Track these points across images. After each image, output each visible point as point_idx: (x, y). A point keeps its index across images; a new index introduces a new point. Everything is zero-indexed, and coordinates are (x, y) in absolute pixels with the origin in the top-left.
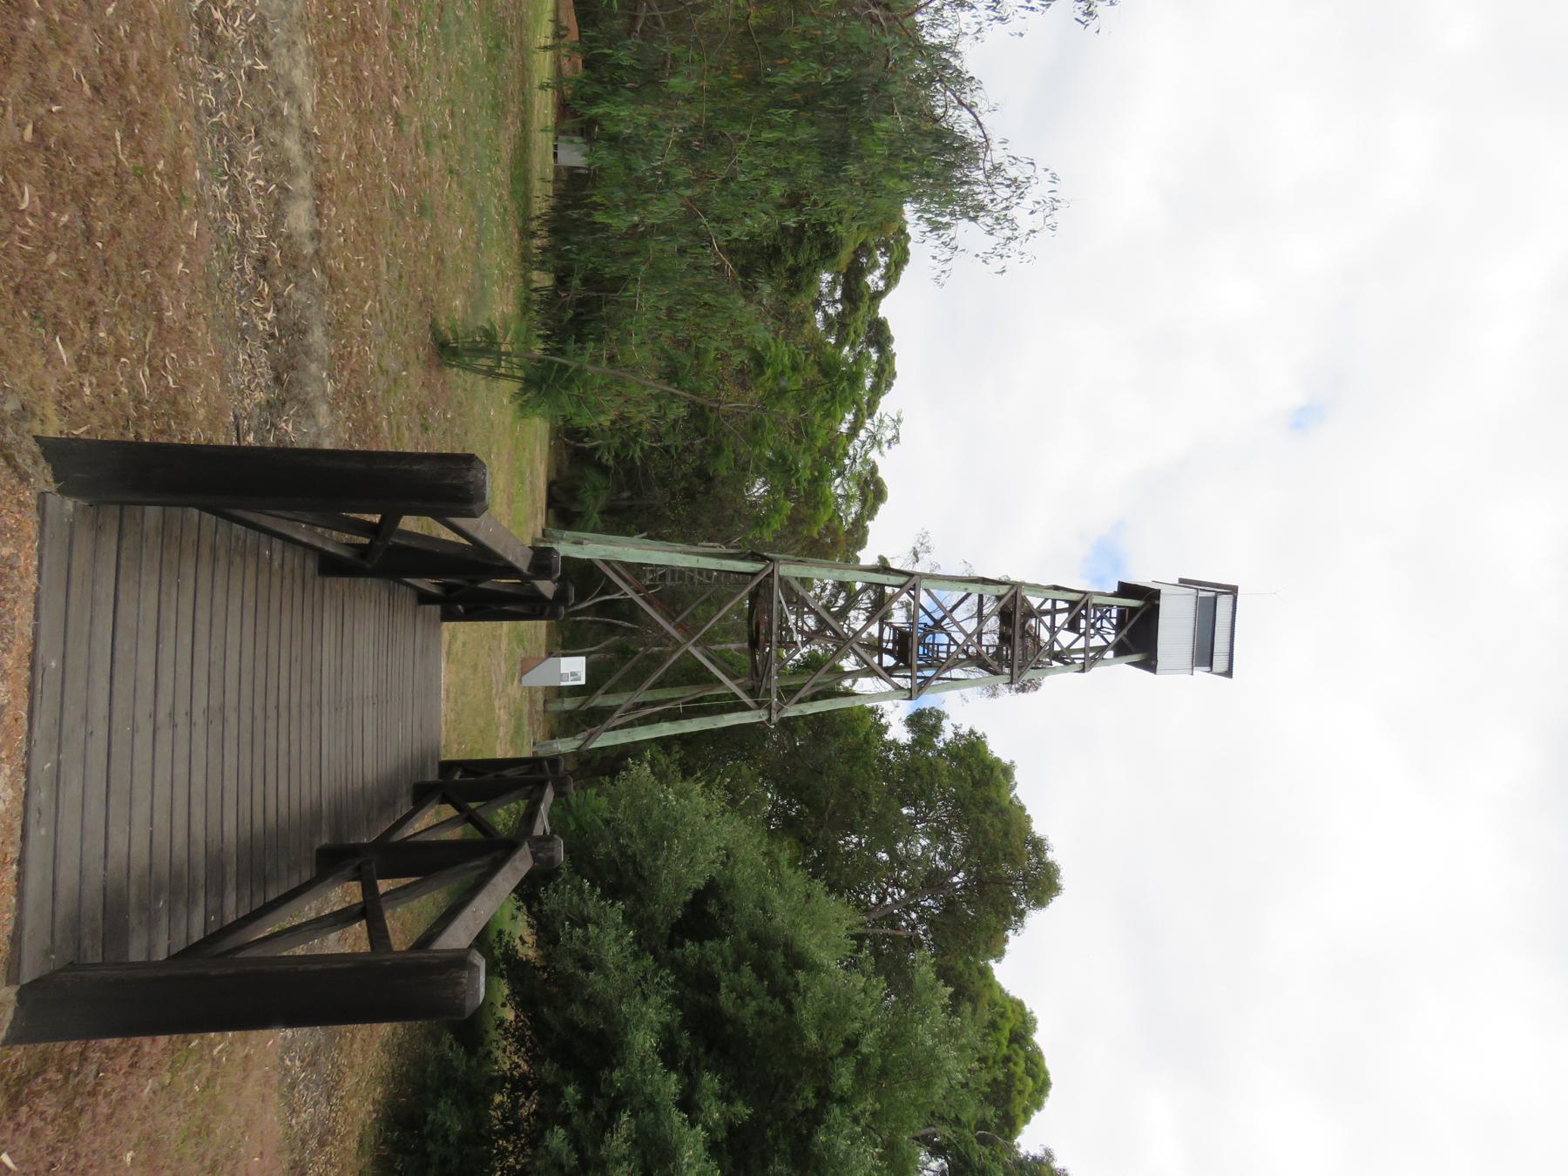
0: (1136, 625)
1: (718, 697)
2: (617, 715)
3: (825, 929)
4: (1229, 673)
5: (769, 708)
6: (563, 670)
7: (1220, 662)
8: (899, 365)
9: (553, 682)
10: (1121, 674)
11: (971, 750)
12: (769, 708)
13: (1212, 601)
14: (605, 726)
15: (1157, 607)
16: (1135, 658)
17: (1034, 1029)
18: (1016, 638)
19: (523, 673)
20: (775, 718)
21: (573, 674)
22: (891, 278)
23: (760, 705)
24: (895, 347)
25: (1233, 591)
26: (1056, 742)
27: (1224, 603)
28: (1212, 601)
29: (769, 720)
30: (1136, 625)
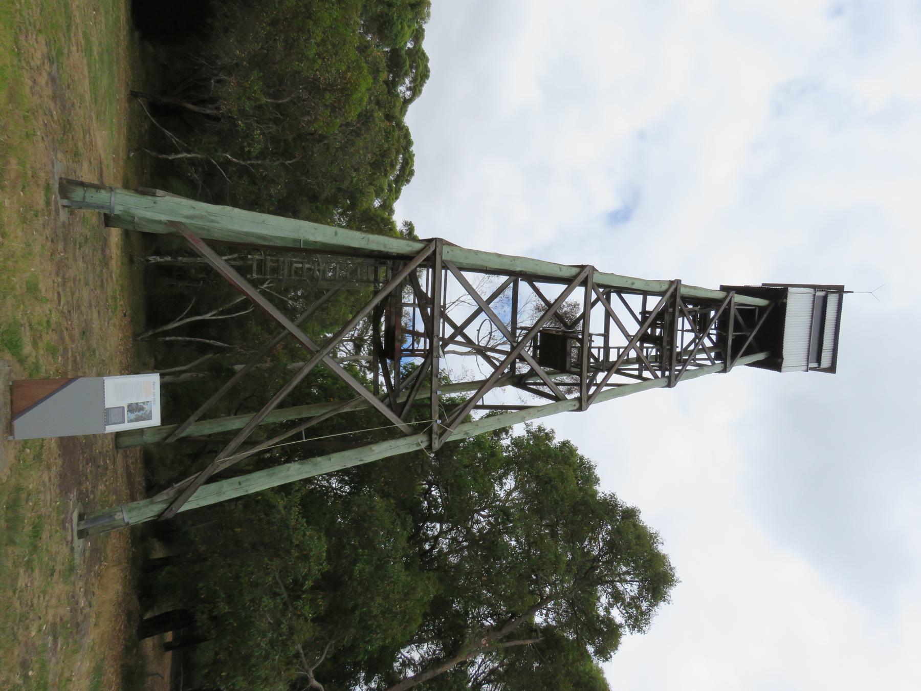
0: (751, 326)
1: (350, 416)
2: (233, 445)
3: (118, 293)
4: (832, 369)
5: (430, 433)
6: (111, 401)
7: (826, 361)
8: (417, 166)
9: (79, 427)
10: (745, 376)
11: (566, 451)
12: (430, 433)
13: (827, 297)
14: (211, 470)
15: (784, 306)
16: (760, 357)
17: (603, 673)
18: (557, 353)
19: (15, 413)
20: (436, 445)
21: (133, 408)
22: (416, 90)
23: (416, 431)
24: (414, 149)
25: (839, 290)
26: (645, 445)
27: (832, 300)
28: (827, 297)
29: (430, 447)
30: (751, 326)
